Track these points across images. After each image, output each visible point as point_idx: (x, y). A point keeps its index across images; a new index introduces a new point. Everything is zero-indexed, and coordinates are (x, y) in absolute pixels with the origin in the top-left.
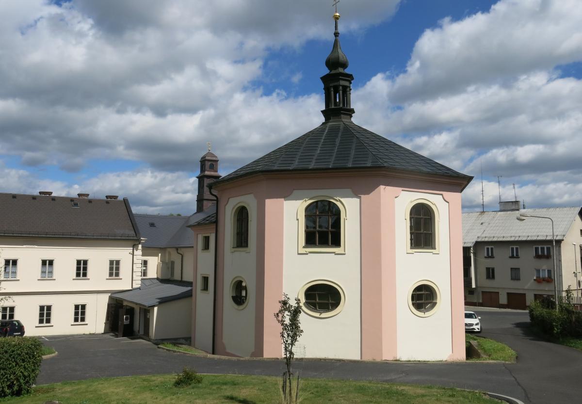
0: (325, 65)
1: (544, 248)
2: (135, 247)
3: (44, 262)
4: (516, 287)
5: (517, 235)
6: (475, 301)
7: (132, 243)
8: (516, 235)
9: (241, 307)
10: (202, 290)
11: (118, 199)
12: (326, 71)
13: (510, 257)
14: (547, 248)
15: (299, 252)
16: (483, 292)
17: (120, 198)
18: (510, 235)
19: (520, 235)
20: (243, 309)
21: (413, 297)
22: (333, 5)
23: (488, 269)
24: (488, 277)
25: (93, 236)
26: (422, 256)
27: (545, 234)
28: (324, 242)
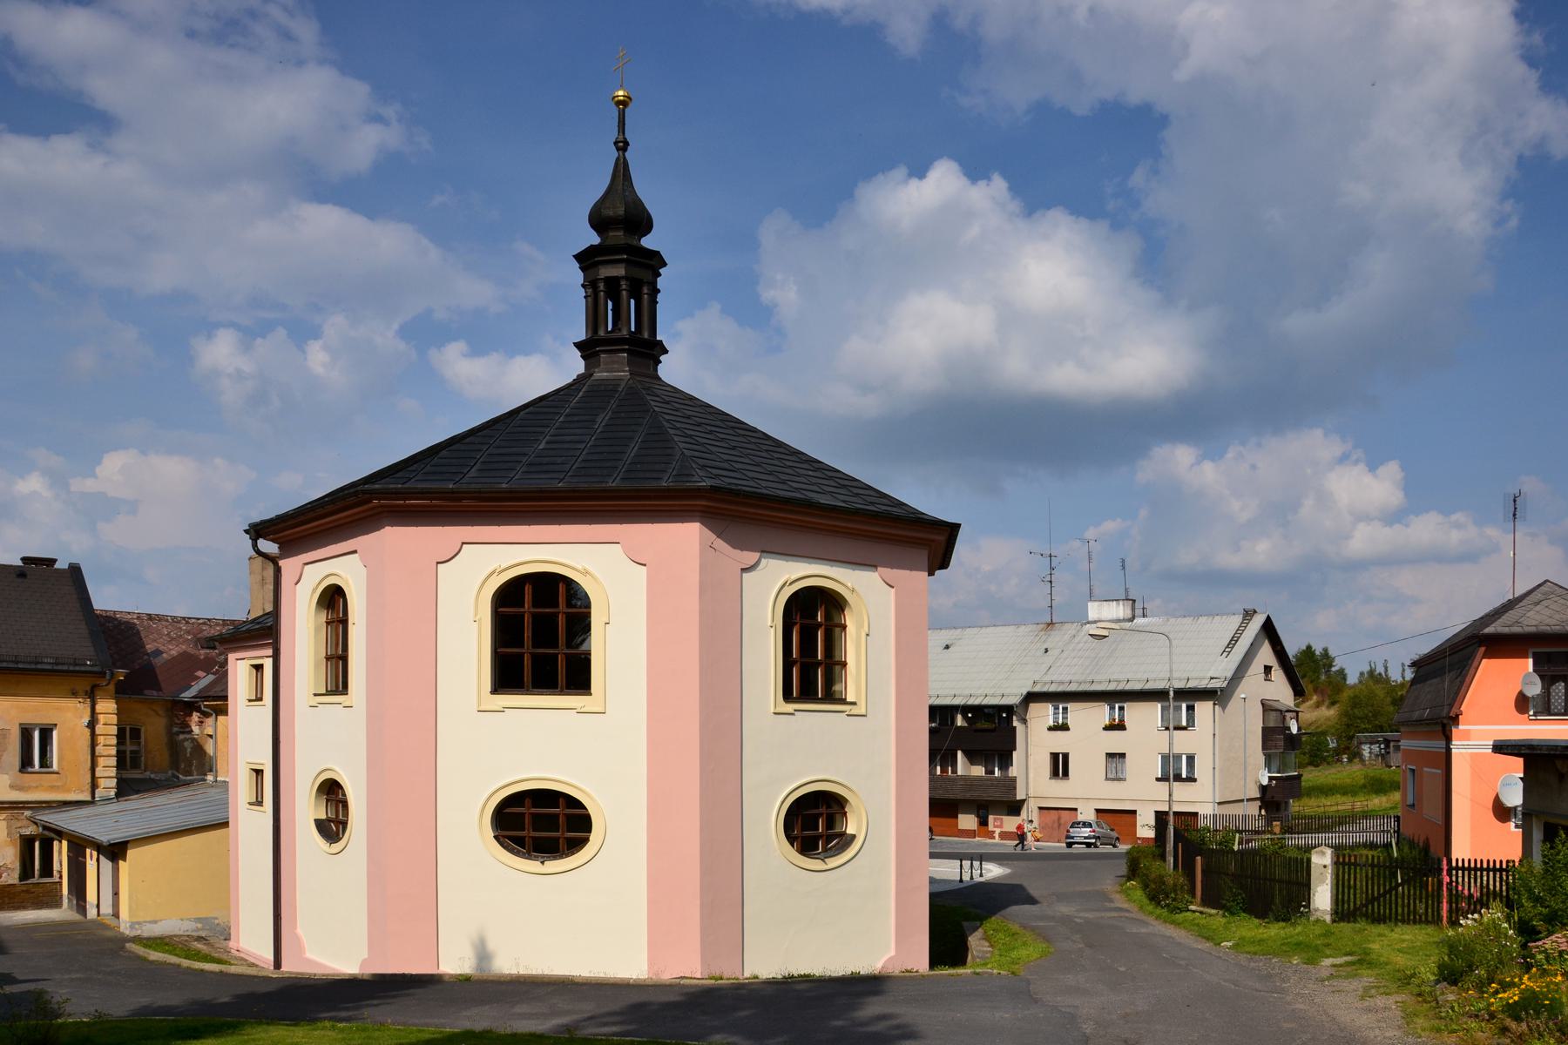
0: (1517, 713)
2: (92, 695)
3: (1110, 756)
4: (1116, 796)
5: (1123, 677)
7: (85, 684)
8: (1121, 677)
9: (337, 847)
11: (57, 566)
17: (61, 564)
18: (1106, 677)
19: (1129, 676)
21: (577, 845)
24: (1055, 773)
25: (17, 663)
26: (813, 719)
27: (1185, 675)
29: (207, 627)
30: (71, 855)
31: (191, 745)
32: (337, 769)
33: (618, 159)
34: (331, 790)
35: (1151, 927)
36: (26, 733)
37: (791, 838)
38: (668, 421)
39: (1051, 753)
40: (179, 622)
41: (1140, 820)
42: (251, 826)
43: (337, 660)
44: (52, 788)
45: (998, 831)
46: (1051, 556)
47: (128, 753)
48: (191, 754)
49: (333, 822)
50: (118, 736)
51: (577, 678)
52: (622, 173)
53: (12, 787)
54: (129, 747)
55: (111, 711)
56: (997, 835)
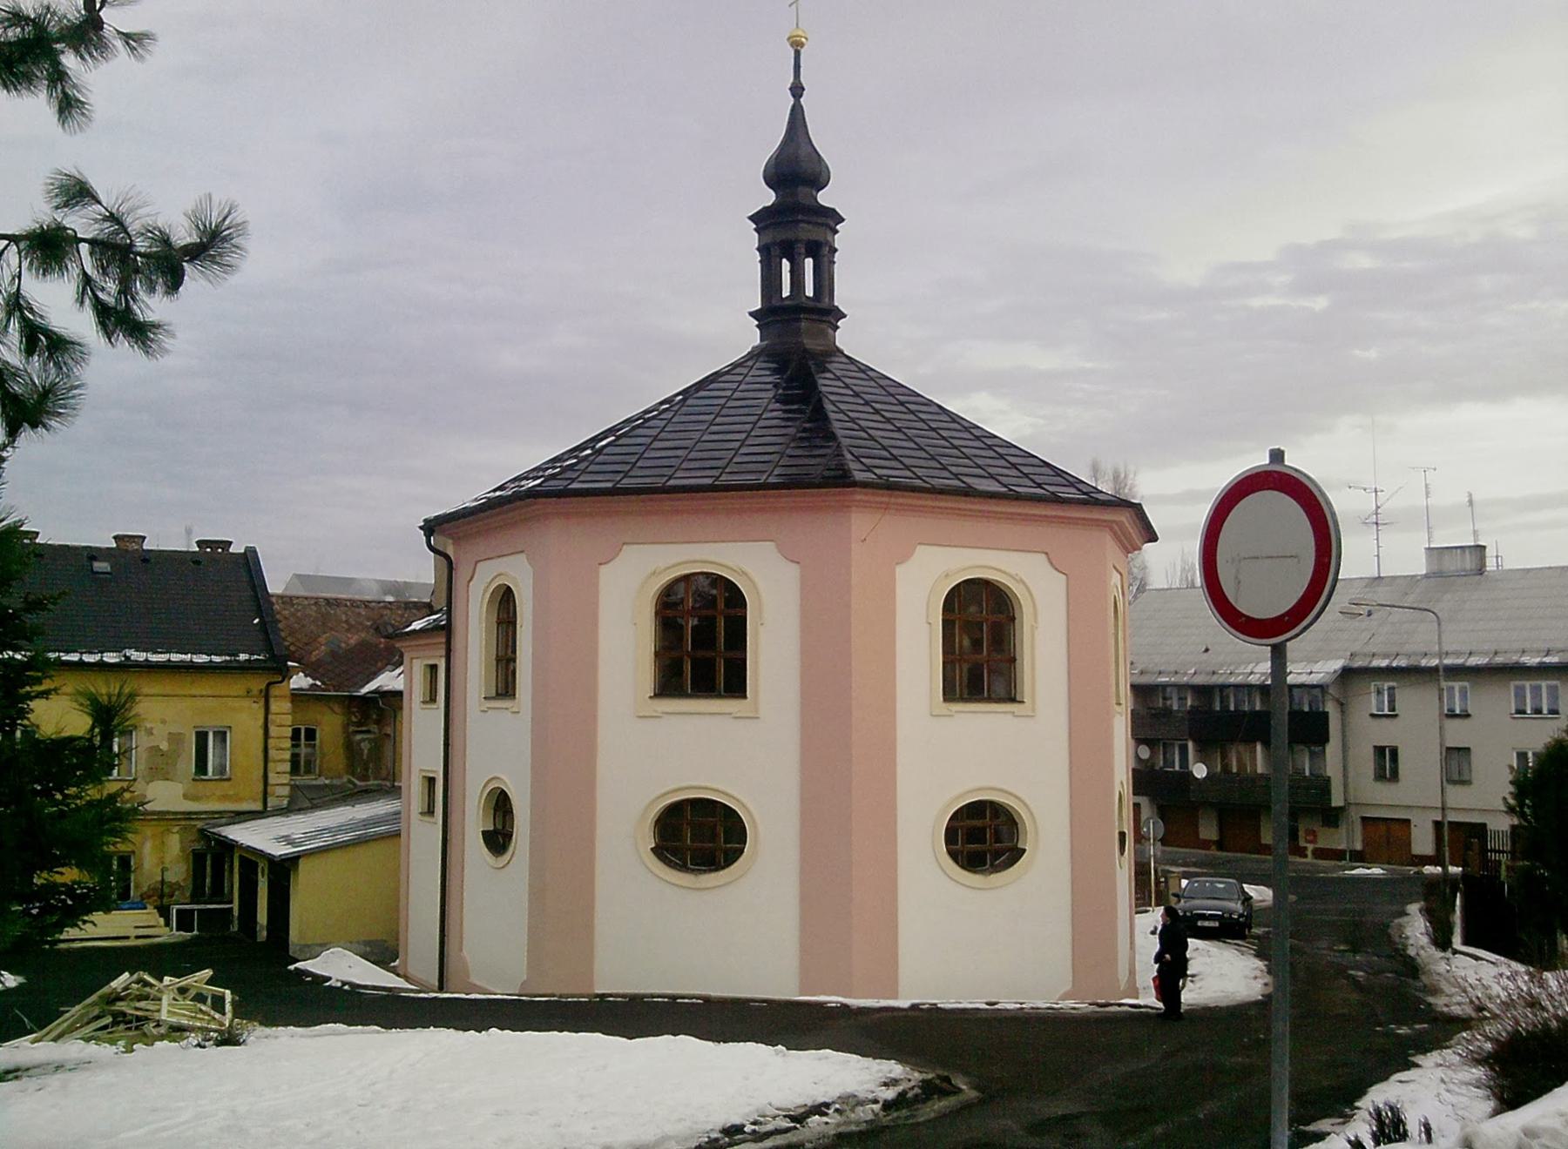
1: (1539, 688)
6: (1342, 847)
10: (421, 813)
12: (769, 197)
13: (651, 697)
14: (1549, 687)
15: (934, 713)
16: (1364, 819)
20: (503, 867)
21: (732, 856)
22: (790, 6)
23: (1380, 751)
24: (1380, 776)
28: (705, 686)
29: (388, 612)
30: (271, 876)
31: (369, 746)
32: (502, 777)
33: (794, 106)
34: (501, 804)
35: (130, 845)
36: (202, 737)
37: (953, 855)
38: (833, 403)
39: (1375, 747)
40: (358, 607)
41: (1415, 833)
42: (424, 837)
43: (505, 662)
44: (225, 798)
45: (1310, 847)
46: (1376, 491)
47: (303, 756)
48: (368, 757)
49: (500, 834)
50: (293, 738)
51: (735, 686)
52: (797, 119)
53: (185, 796)
54: (303, 750)
55: (286, 711)
56: (1309, 853)
